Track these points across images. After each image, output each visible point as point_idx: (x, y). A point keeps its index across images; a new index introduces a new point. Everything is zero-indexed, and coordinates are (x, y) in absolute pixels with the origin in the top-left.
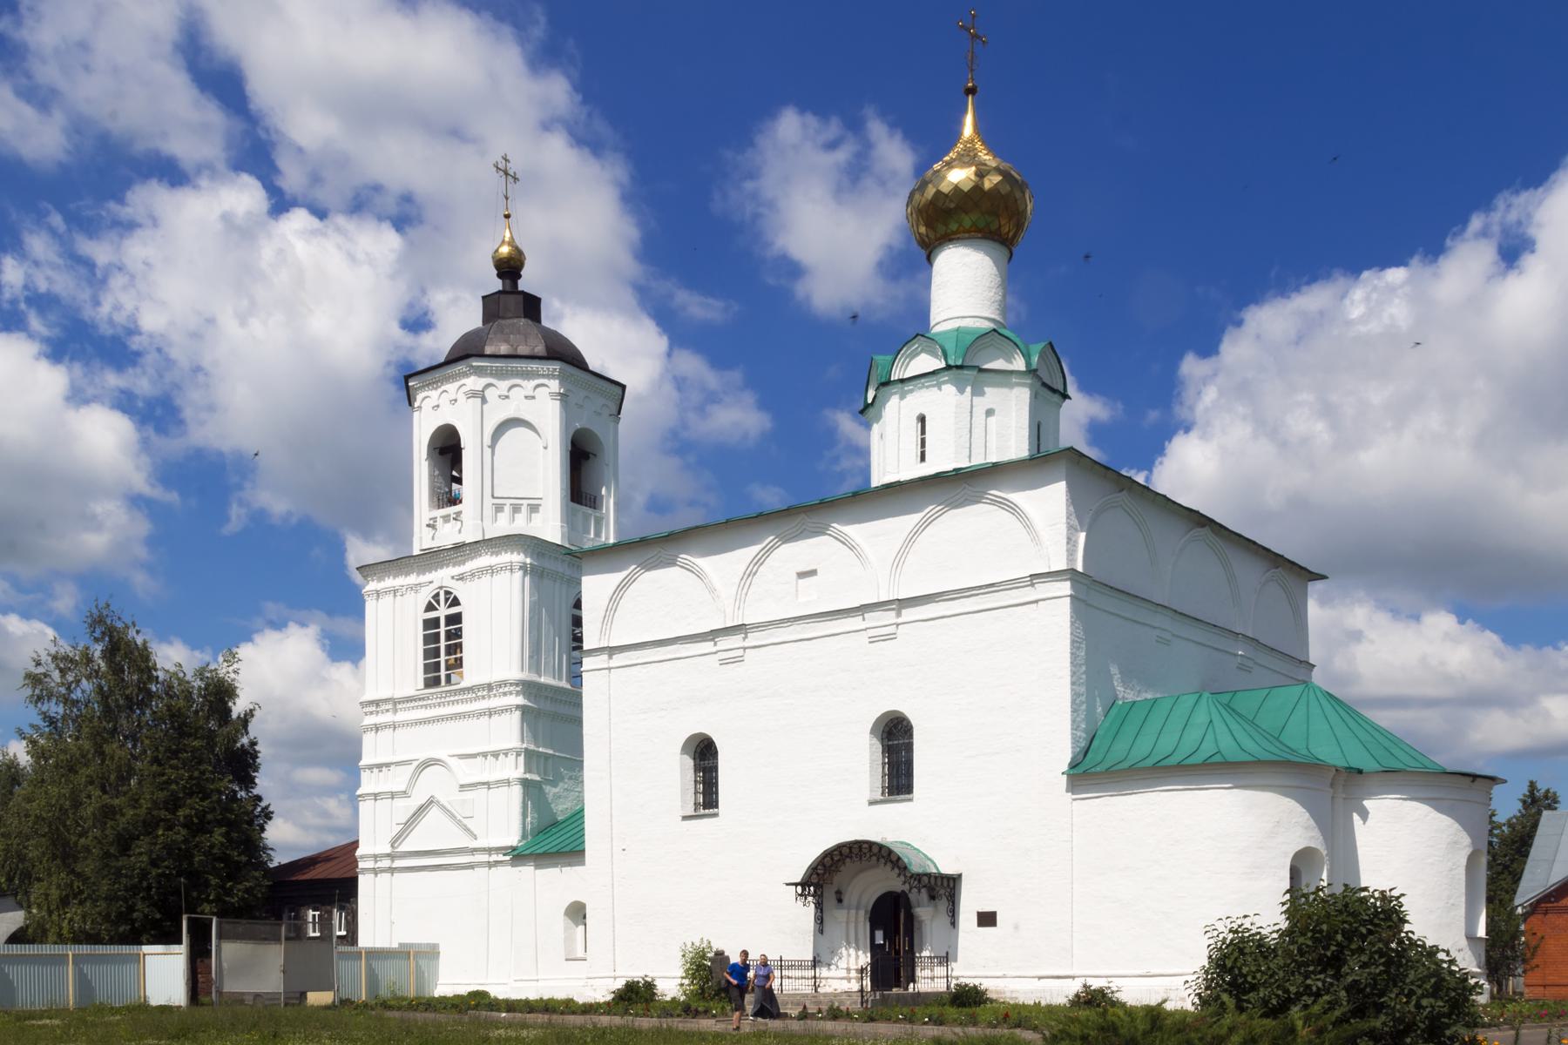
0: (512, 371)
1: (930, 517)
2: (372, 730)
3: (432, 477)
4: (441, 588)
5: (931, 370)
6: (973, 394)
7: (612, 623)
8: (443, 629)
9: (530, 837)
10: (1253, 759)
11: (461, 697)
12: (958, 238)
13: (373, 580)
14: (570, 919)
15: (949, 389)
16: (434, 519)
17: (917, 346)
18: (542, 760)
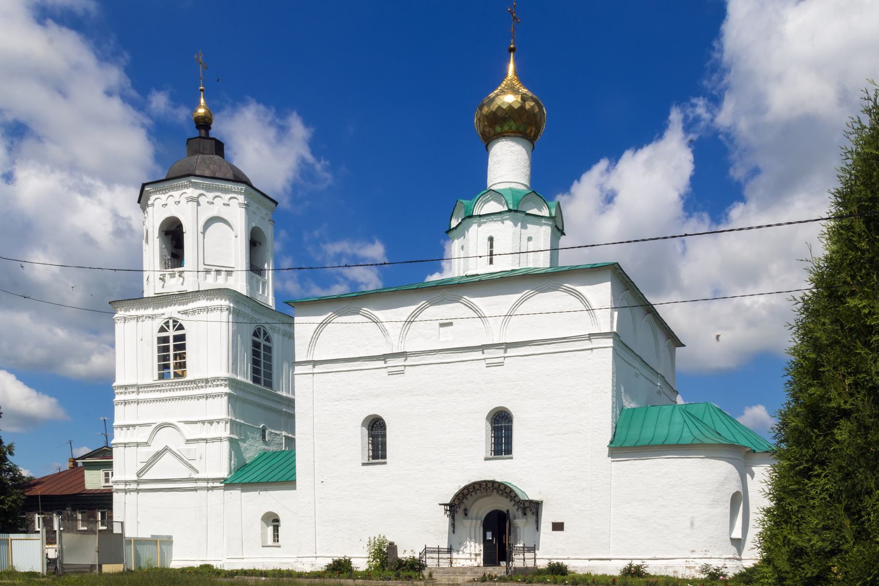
0: (216, 187)
1: (526, 296)
2: (122, 404)
3: (161, 248)
4: (170, 318)
5: (499, 211)
6: (522, 228)
7: (315, 346)
8: (171, 344)
9: (233, 473)
10: (699, 442)
11: (186, 386)
12: (508, 136)
13: (121, 311)
14: (264, 522)
15: (509, 223)
17: (489, 196)
18: (238, 427)
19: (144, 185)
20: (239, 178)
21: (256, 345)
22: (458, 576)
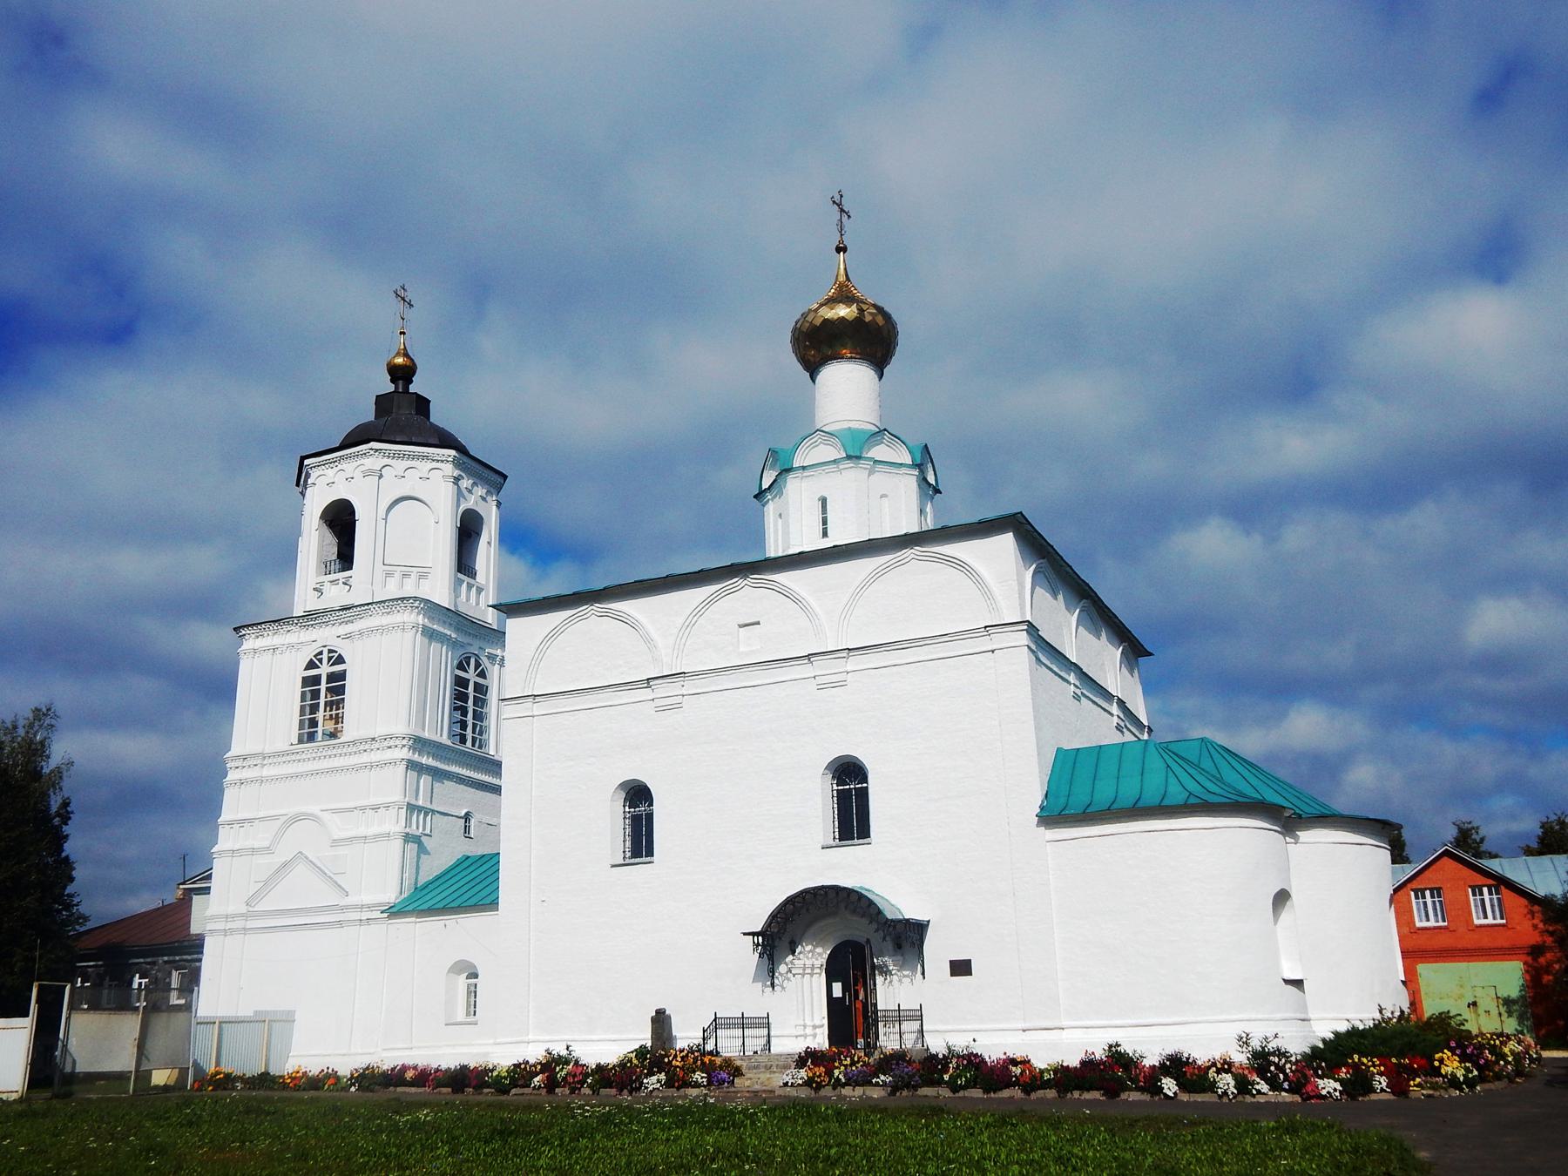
8: (323, 686)
10: (1199, 801)
19: (303, 458)
20: (444, 440)
21: (461, 682)
22: (774, 1072)
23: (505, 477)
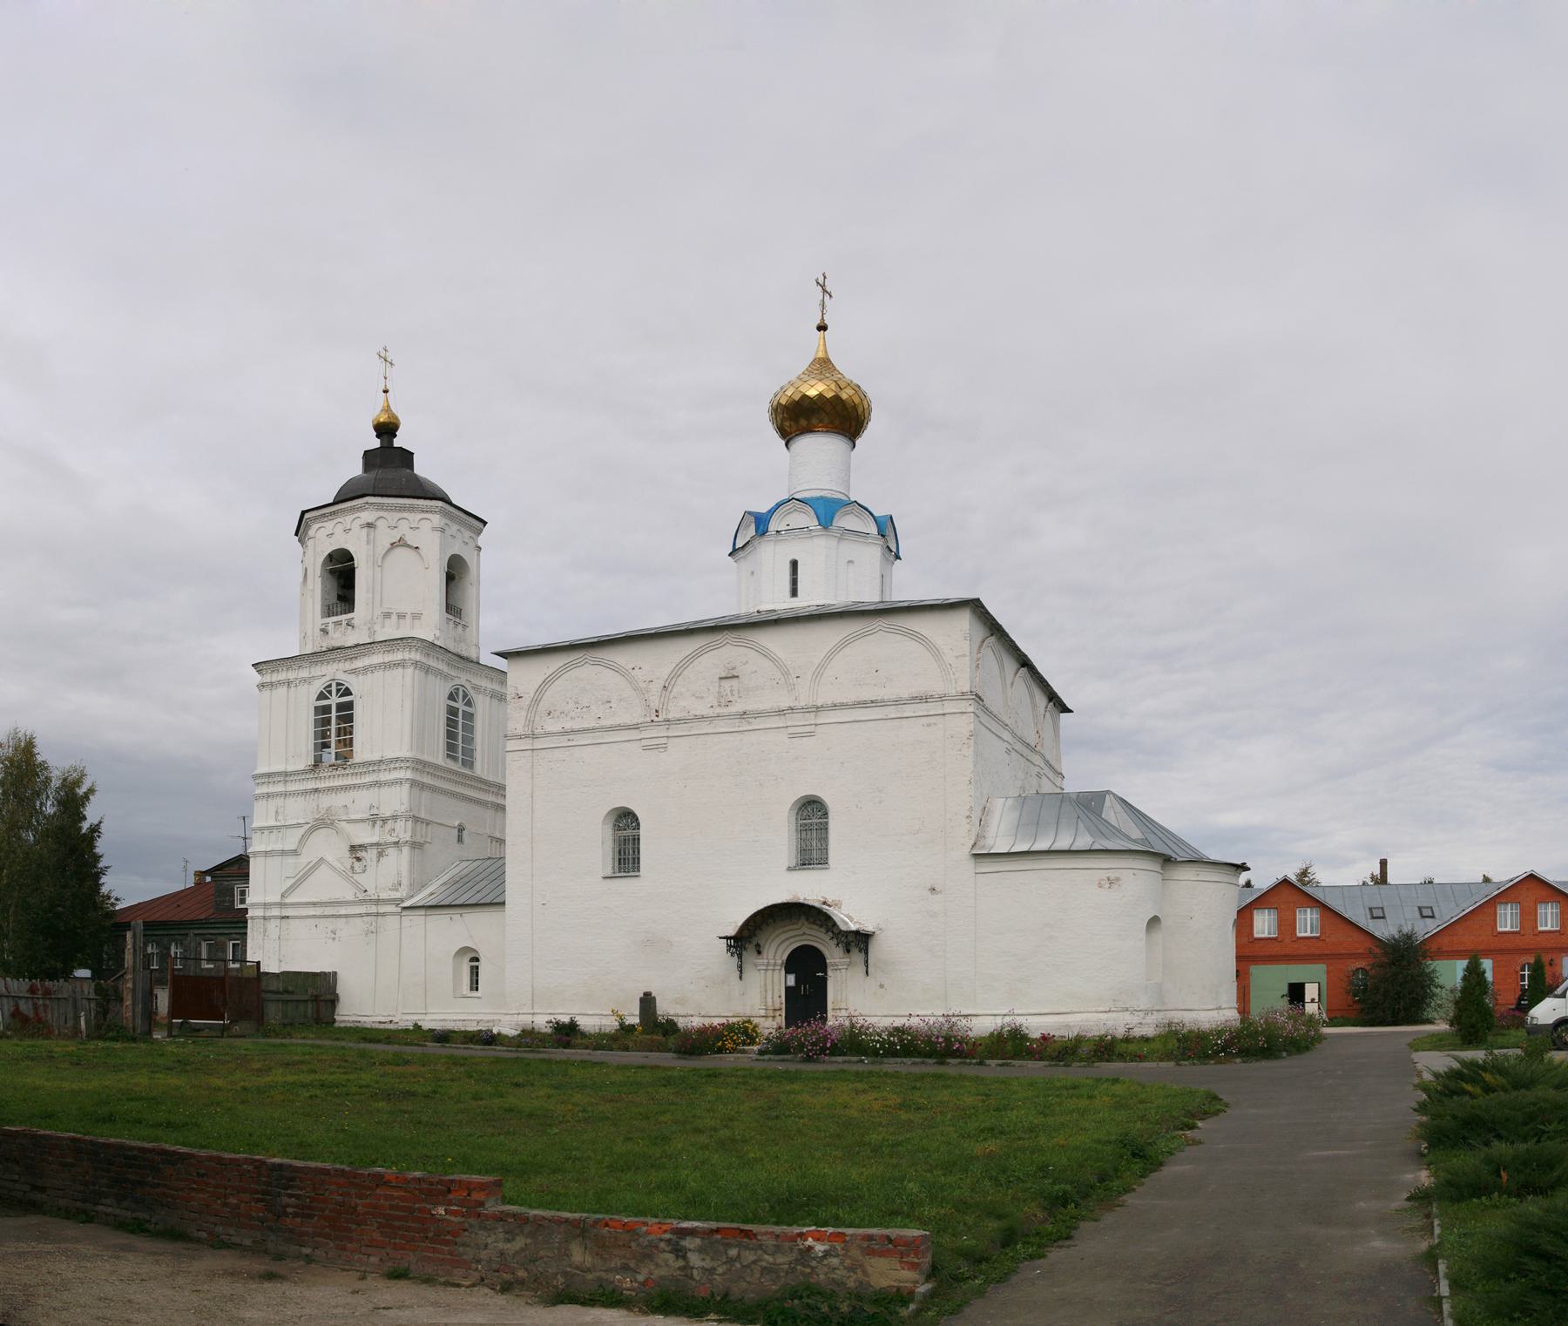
8: (334, 714)
16: (327, 624)
19: (303, 513)
21: (452, 712)
23: (485, 523)
